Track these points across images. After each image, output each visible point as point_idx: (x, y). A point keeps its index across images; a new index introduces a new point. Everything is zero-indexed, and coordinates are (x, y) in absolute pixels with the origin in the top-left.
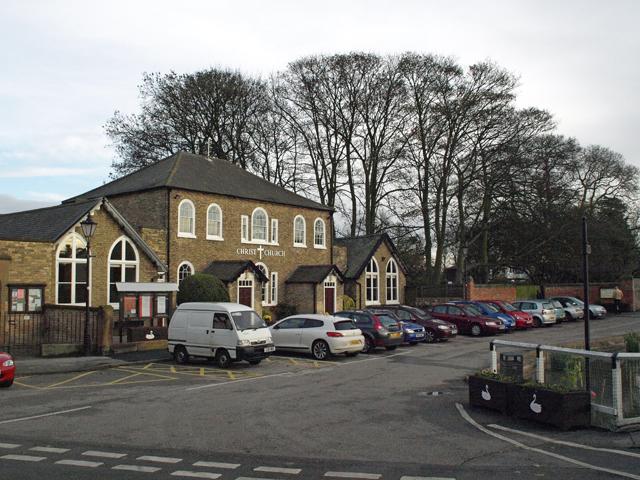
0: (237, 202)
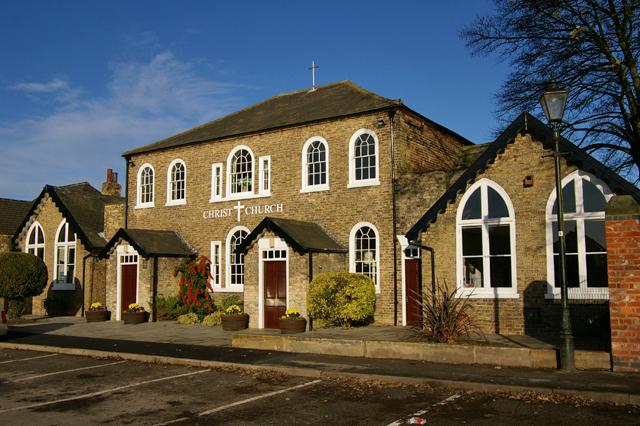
0: (207, 148)
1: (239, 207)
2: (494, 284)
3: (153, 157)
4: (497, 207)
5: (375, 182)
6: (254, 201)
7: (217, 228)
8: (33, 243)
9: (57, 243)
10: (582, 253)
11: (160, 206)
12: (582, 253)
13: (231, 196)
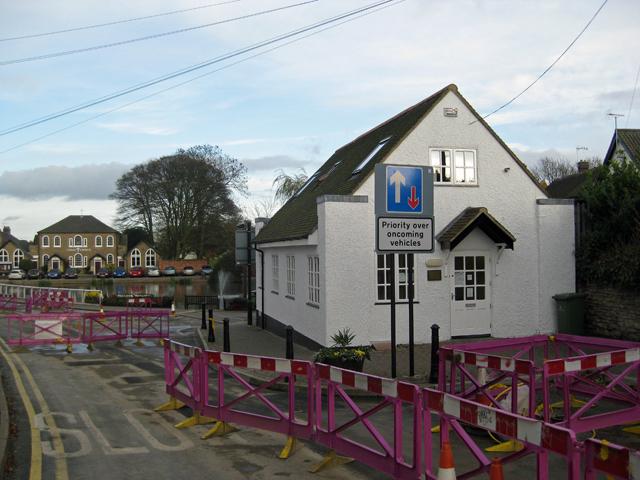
7: (72, 253)
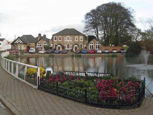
1: (68, 42)
2: (98, 48)
3: (57, 36)
4: (40, 43)
5: (82, 41)
6: (70, 41)
7: (66, 43)
8: (40, 45)
9: (93, 45)
10: (92, 47)
11: (58, 41)
12: (92, 47)
13: (67, 41)
